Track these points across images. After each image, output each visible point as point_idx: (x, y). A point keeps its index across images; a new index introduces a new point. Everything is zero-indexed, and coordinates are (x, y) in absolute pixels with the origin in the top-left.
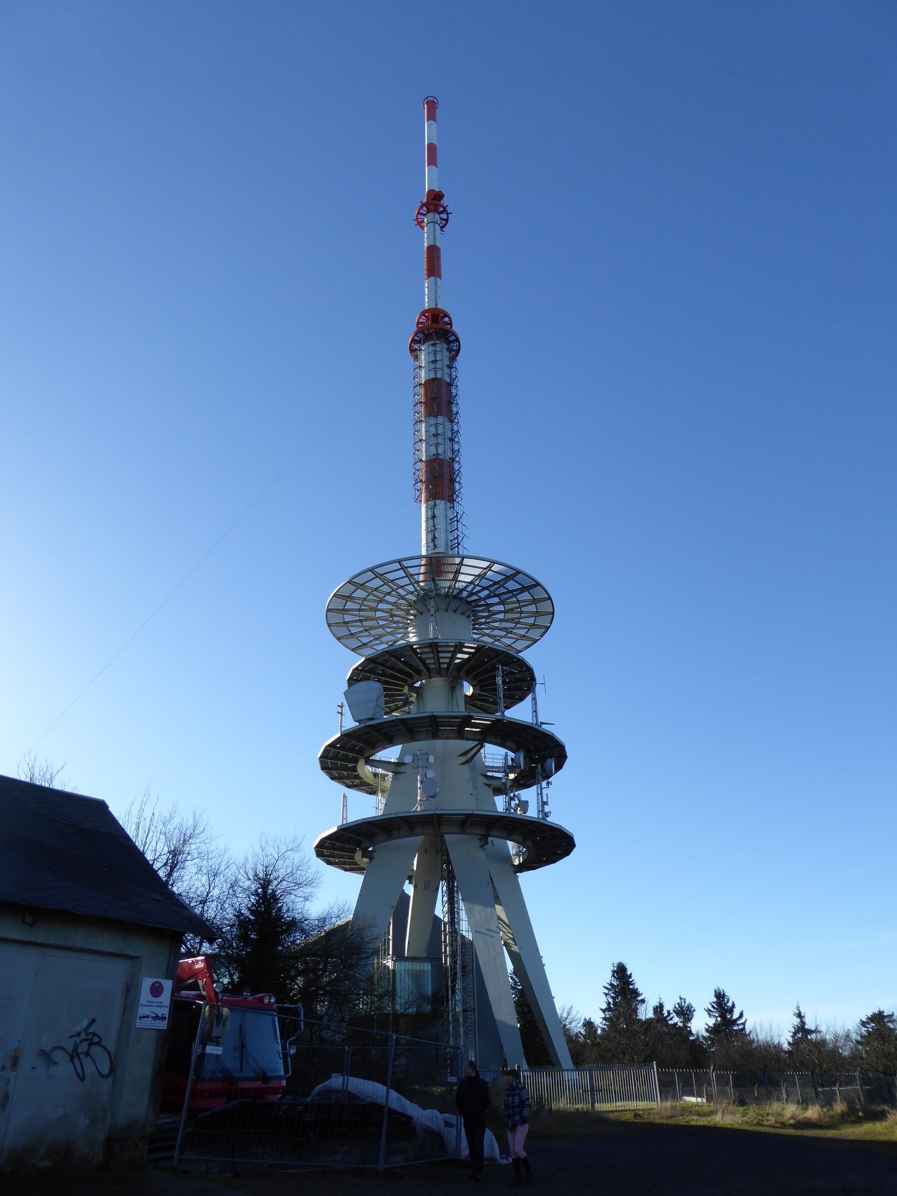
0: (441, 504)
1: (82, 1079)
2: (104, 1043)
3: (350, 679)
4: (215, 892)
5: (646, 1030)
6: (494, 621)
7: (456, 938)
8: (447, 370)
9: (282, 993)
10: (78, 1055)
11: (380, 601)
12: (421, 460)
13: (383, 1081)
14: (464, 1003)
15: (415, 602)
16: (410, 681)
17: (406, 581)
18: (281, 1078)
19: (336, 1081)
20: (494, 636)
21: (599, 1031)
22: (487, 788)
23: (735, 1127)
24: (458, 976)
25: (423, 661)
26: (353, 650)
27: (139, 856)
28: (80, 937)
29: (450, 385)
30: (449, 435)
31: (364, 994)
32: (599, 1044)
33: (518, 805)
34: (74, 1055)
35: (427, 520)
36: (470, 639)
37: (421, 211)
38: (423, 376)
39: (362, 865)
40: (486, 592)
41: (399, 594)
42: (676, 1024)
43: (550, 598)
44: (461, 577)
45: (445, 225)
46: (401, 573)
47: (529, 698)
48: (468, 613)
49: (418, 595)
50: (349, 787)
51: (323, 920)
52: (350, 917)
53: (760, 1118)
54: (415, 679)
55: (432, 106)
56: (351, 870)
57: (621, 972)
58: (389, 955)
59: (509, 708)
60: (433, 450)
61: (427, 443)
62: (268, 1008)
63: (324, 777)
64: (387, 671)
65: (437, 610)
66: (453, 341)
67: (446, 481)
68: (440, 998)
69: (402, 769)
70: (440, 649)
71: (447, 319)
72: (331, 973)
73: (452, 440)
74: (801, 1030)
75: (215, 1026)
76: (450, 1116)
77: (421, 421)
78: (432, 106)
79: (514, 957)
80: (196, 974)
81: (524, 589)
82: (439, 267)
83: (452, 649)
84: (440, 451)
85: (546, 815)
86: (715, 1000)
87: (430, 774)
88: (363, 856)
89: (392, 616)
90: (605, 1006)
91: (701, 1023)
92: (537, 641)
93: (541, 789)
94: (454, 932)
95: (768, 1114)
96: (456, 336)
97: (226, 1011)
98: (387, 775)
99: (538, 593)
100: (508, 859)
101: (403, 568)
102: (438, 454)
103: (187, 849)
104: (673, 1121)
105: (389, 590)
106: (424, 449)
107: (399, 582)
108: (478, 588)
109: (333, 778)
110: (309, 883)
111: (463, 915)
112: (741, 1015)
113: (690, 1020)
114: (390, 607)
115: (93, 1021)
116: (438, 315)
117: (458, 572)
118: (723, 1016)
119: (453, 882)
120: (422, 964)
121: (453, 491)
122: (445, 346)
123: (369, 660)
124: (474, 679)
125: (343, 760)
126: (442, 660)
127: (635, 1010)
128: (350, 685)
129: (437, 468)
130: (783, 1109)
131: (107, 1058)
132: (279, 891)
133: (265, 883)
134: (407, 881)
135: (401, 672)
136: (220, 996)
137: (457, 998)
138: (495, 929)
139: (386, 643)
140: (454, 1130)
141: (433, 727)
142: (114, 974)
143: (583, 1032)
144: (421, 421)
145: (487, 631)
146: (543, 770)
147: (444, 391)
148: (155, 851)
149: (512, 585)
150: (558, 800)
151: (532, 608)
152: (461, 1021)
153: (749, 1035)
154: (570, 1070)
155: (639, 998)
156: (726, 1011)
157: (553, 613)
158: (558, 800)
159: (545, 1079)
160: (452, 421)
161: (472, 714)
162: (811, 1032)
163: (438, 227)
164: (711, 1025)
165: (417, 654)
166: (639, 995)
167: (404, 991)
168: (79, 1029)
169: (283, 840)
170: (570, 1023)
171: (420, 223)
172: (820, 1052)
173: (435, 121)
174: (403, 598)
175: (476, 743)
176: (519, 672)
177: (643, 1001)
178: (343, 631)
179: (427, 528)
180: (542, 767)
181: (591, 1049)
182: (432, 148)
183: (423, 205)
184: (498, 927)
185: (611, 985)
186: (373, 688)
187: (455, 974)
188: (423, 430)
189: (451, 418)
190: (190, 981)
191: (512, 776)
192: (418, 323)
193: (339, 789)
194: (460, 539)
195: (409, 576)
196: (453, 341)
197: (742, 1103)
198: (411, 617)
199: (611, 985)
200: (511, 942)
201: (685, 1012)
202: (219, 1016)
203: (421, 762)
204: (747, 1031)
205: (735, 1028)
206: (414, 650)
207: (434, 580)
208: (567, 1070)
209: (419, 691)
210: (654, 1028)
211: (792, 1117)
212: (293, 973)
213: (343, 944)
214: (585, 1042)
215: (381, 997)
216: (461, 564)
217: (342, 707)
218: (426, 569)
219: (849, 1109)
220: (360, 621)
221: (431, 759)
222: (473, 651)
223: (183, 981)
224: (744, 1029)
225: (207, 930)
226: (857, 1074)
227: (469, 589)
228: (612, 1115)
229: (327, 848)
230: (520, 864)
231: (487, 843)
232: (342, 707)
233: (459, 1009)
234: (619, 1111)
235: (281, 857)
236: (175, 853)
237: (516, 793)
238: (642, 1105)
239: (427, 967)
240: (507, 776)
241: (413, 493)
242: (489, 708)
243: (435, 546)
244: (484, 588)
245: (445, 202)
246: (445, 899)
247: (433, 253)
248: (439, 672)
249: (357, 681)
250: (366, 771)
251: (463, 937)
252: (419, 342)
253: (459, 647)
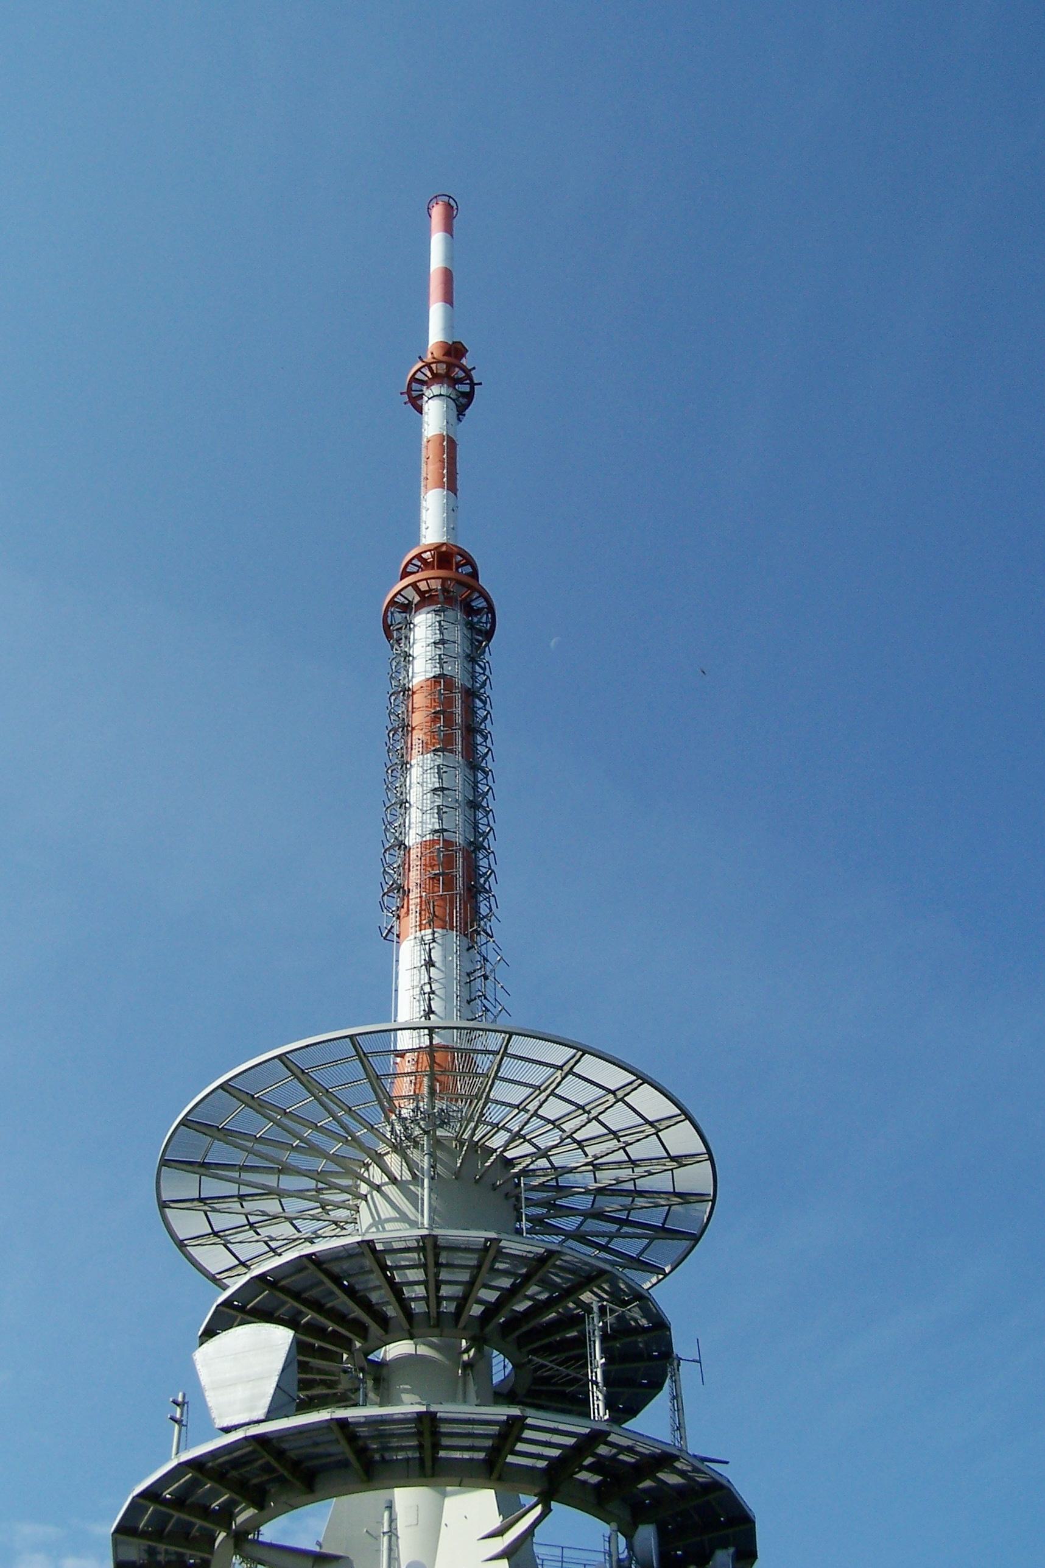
47: (662, 1398)
66: (478, 612)
96: (487, 599)
135: (340, 1317)
208: (594, 1200)
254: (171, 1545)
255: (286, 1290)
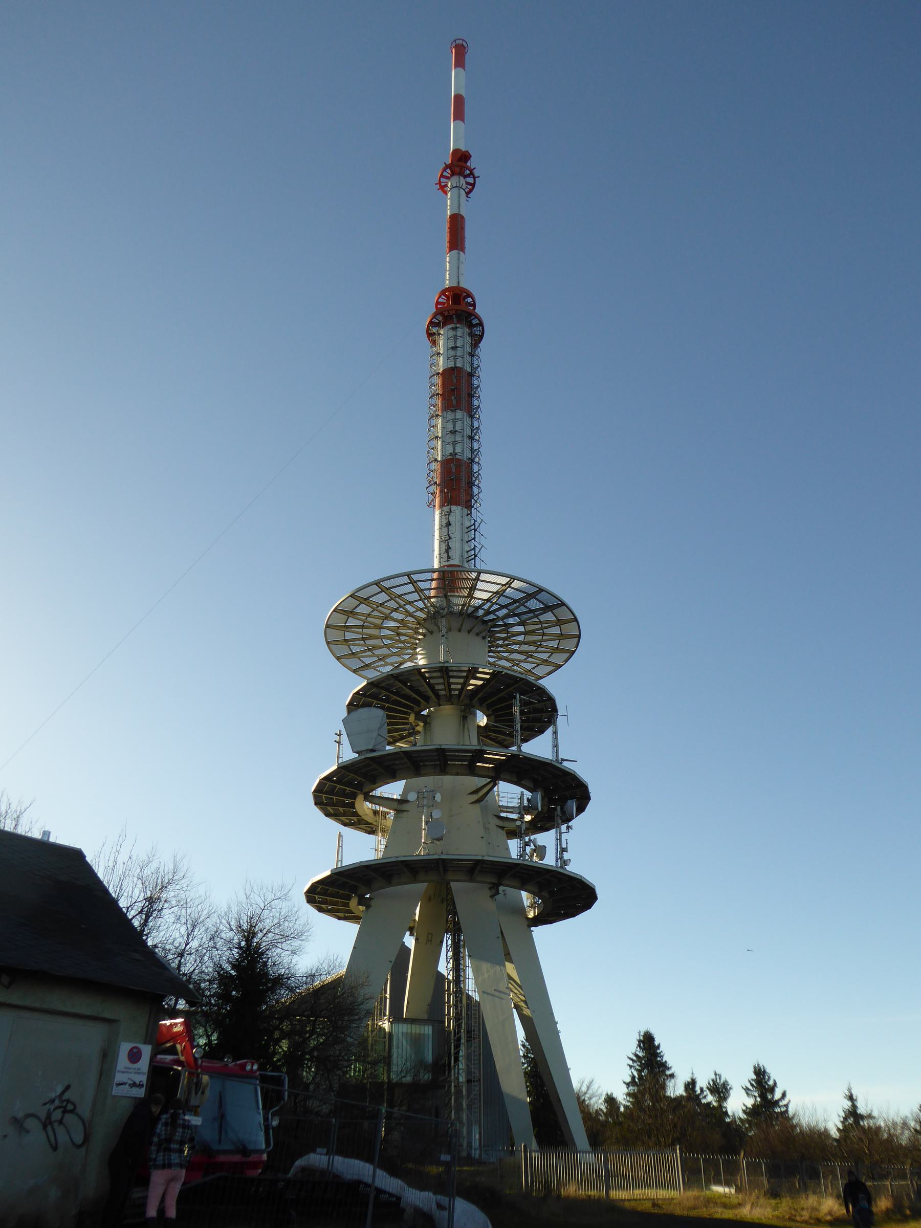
0: (457, 510)
1: (55, 1148)
2: (79, 1110)
3: (350, 704)
4: (194, 944)
5: (674, 1110)
6: (514, 644)
7: (461, 998)
8: (468, 358)
9: (263, 1056)
10: (51, 1123)
11: (386, 618)
12: (436, 460)
13: (369, 1160)
14: (469, 1072)
15: (425, 620)
16: (416, 708)
17: (415, 596)
18: (262, 1152)
19: (317, 1159)
20: (513, 660)
21: (622, 1109)
22: (499, 829)
23: (764, 1221)
24: (463, 1041)
25: (432, 687)
26: (354, 671)
27: (113, 903)
28: (57, 999)
29: (471, 375)
30: (468, 432)
31: (356, 1061)
32: (621, 1124)
33: (534, 851)
34: (47, 1123)
35: (440, 529)
36: (485, 663)
37: (445, 174)
38: (442, 364)
39: (357, 914)
40: (505, 611)
41: (407, 611)
42: (709, 1103)
43: (576, 620)
44: (477, 594)
45: (471, 191)
46: (410, 588)
47: (550, 731)
48: (484, 634)
49: (429, 612)
50: (345, 825)
51: (312, 976)
52: (343, 971)
53: (793, 1212)
54: (422, 707)
55: (461, 51)
56: (345, 918)
57: (648, 1042)
58: (385, 1015)
59: (527, 741)
60: (450, 449)
61: (443, 441)
62: (250, 1075)
63: (318, 813)
64: (390, 698)
65: (449, 630)
66: (476, 325)
67: (464, 484)
68: (441, 1067)
69: (405, 807)
70: (451, 674)
71: (470, 300)
72: (320, 1035)
73: (471, 438)
74: (853, 1114)
75: (193, 1094)
76: (442, 1197)
77: (437, 415)
78: (461, 51)
79: (527, 1023)
80: (176, 1037)
81: (547, 608)
82: (463, 239)
83: (465, 674)
84: (458, 449)
85: (565, 863)
86: (754, 1077)
87: (437, 814)
88: (359, 904)
89: (399, 634)
90: (628, 1080)
91: (738, 1104)
92: (560, 666)
93: (560, 833)
94: (459, 992)
95: (803, 1209)
96: (480, 320)
97: (205, 1078)
98: (389, 813)
99: (563, 613)
100: (522, 911)
101: (412, 582)
102: (456, 454)
103: (164, 896)
104: (694, 1213)
105: (395, 606)
106: (439, 448)
107: (407, 597)
108: (495, 607)
109: (328, 815)
110: (299, 935)
111: (469, 972)
112: (784, 1095)
113: (725, 1099)
114: (397, 624)
115: (68, 1088)
116: (460, 295)
117: (473, 588)
118: (763, 1096)
119: (459, 936)
120: (422, 1027)
121: (471, 496)
122: (467, 330)
123: (371, 684)
124: (488, 708)
125: (339, 795)
126: (453, 686)
127: (663, 1087)
128: (349, 712)
129: (454, 469)
130: (820, 1204)
131: (81, 1128)
132: (264, 944)
133: (249, 935)
134: (408, 933)
136: (200, 1062)
137: (461, 1066)
138: (504, 990)
139: (391, 664)
140: (446, 1213)
141: (440, 761)
142: (90, 1037)
143: (604, 1110)
144: (437, 415)
145: (505, 655)
146: (563, 812)
147: (464, 381)
148: (129, 898)
149: (533, 604)
150: (578, 844)
151: (556, 630)
152: (464, 1092)
153: (793, 1118)
154: (586, 1152)
155: (668, 1073)
156: (766, 1090)
157: (579, 636)
158: (578, 844)
159: (556, 1162)
160: (471, 417)
161: (485, 748)
162: (862, 1117)
163: (463, 193)
164: (750, 1106)
165: (425, 678)
166: (669, 1069)
167: (401, 1055)
168: (53, 1095)
169: (270, 888)
170: (590, 1099)
171: (443, 188)
172: (871, 1141)
173: (464, 68)
174: (411, 615)
175: (489, 780)
176: (539, 701)
177: (672, 1076)
178: (343, 650)
179: (440, 536)
180: (562, 809)
181: (614, 1129)
182: (459, 99)
183: (447, 166)
184: (507, 988)
185: (636, 1055)
186: (375, 716)
187: (459, 1039)
188: (440, 426)
189: (471, 412)
190: (168, 1045)
191: (528, 818)
192: (438, 303)
193: (333, 827)
194: (477, 550)
195: (418, 590)
196: (476, 325)
197: (774, 1194)
198: (420, 637)
199: (636, 1055)
200: (522, 1004)
201: (720, 1090)
202: (198, 1084)
203: (426, 799)
204: (791, 1112)
205: (777, 1110)
206: (422, 675)
207: (446, 596)
209: (426, 720)
210: (684, 1107)
211: (830, 1213)
212: (277, 1034)
213: (333, 1003)
214: (606, 1121)
215: (375, 1063)
216: (477, 579)
217: (340, 735)
218: (438, 584)
219: (895, 1205)
220: (363, 639)
221: (438, 797)
222: (488, 677)
223: (162, 1043)
224: (787, 1111)
225: (182, 986)
226: (907, 1167)
227: (486, 607)
228: (627, 1204)
229: (319, 894)
230: (535, 916)
231: (498, 893)
232: (340, 735)
233: (462, 1079)
234: (636, 1200)
235: (268, 906)
236: (151, 900)
237: (532, 837)
238: (662, 1194)
239: (428, 1030)
240: (523, 818)
241: (427, 497)
242: (505, 740)
243: (449, 557)
244: (502, 607)
245: (471, 164)
246: (450, 954)
247: (457, 224)
248: (450, 699)
249: (358, 707)
250: (365, 807)
251: (469, 997)
252: (437, 325)
253: (472, 673)
254: (175, 1019)
255: (382, 688)
